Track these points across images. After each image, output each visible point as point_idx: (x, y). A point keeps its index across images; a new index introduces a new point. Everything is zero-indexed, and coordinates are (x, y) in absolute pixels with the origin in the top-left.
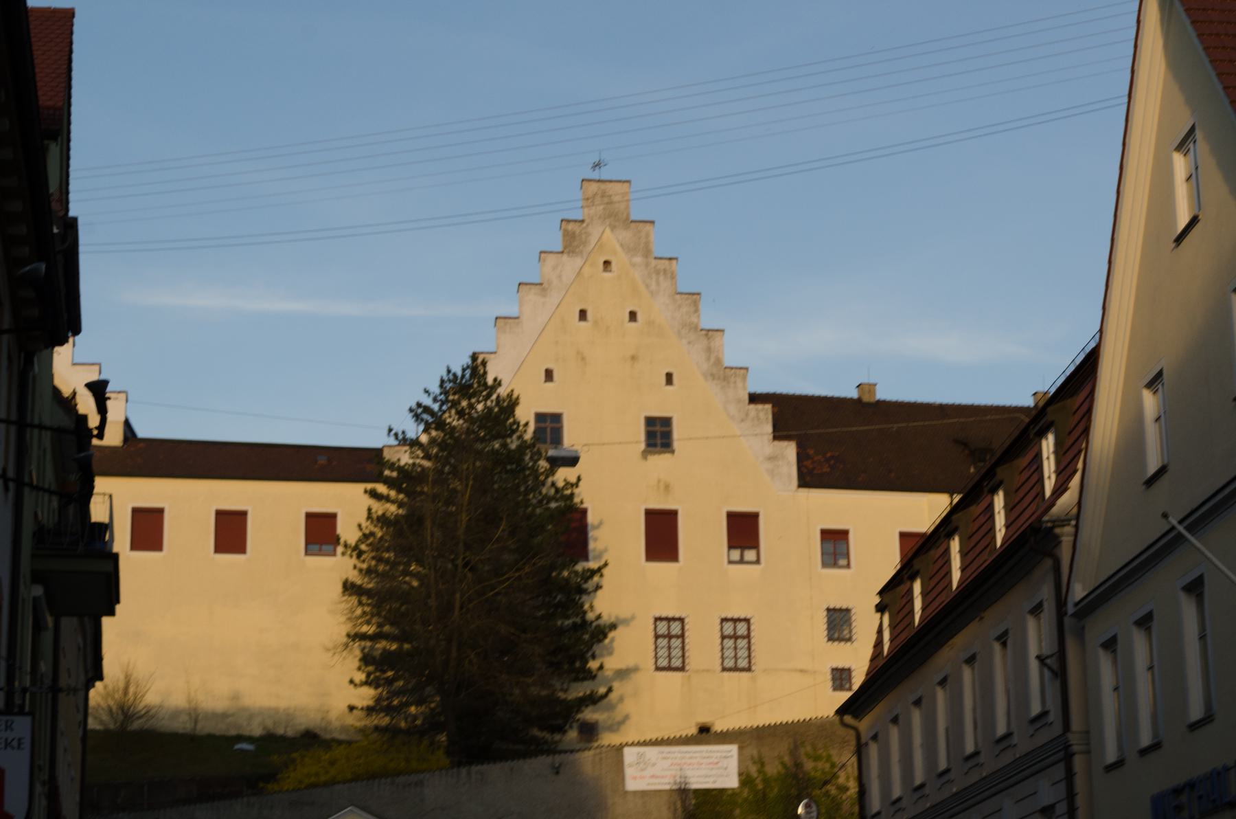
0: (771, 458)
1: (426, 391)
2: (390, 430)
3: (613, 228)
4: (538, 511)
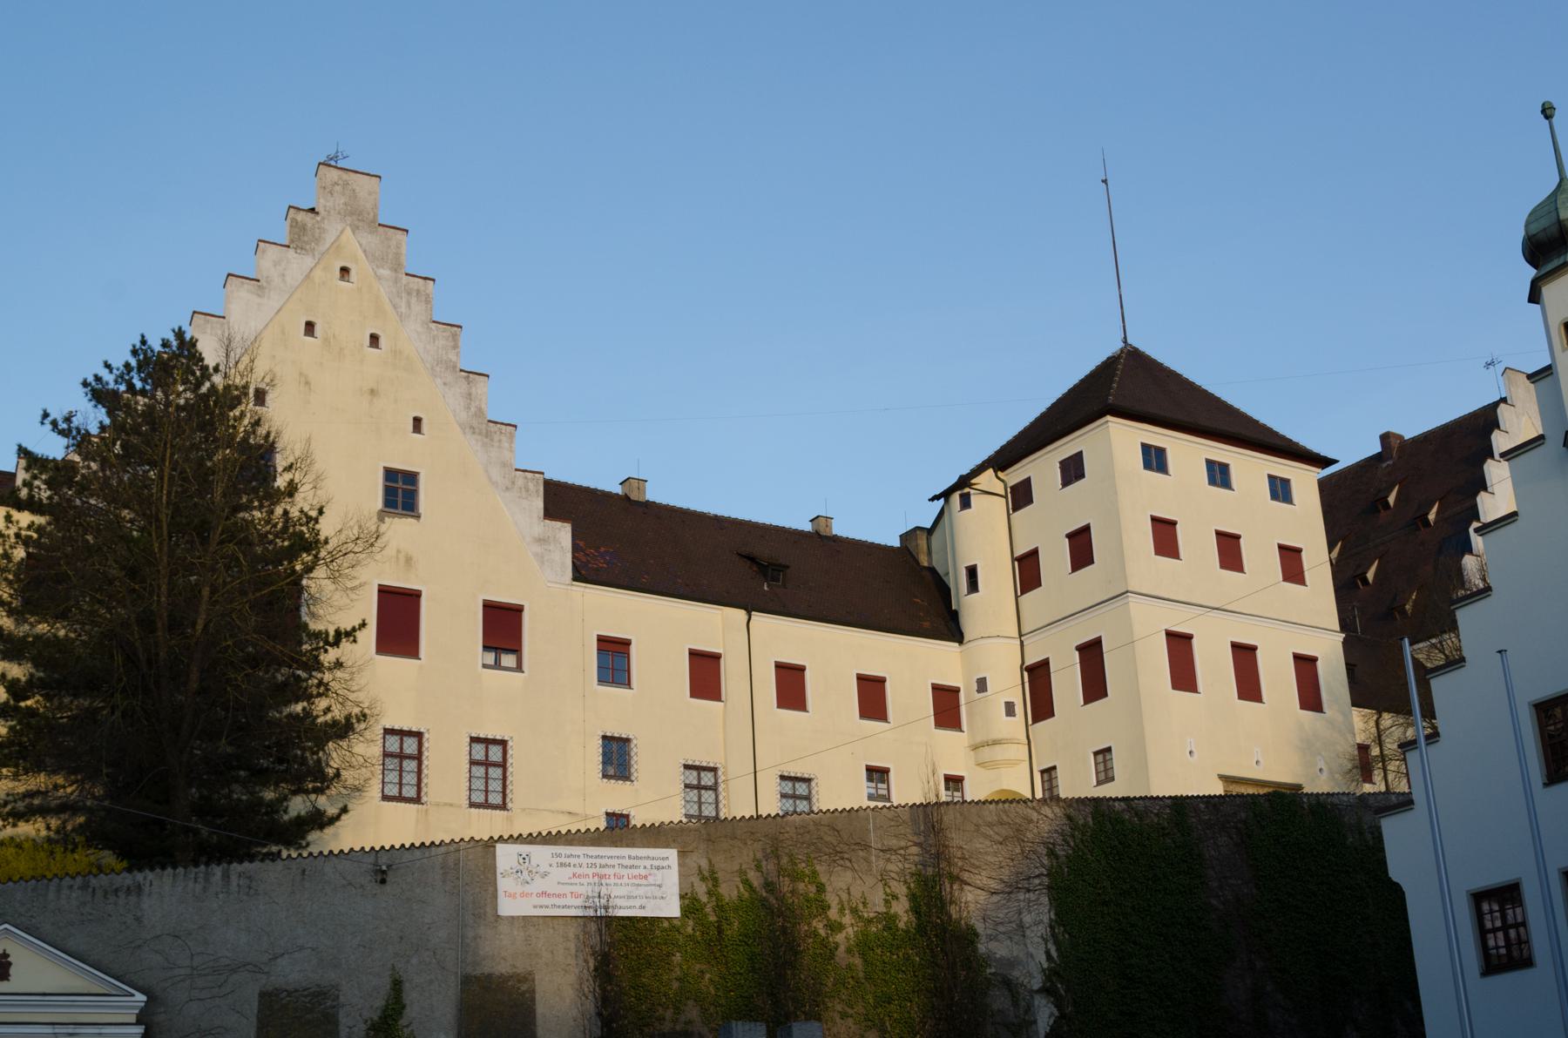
0: (541, 541)
1: (107, 366)
2: (46, 415)
3: (355, 229)
4: (66, 700)
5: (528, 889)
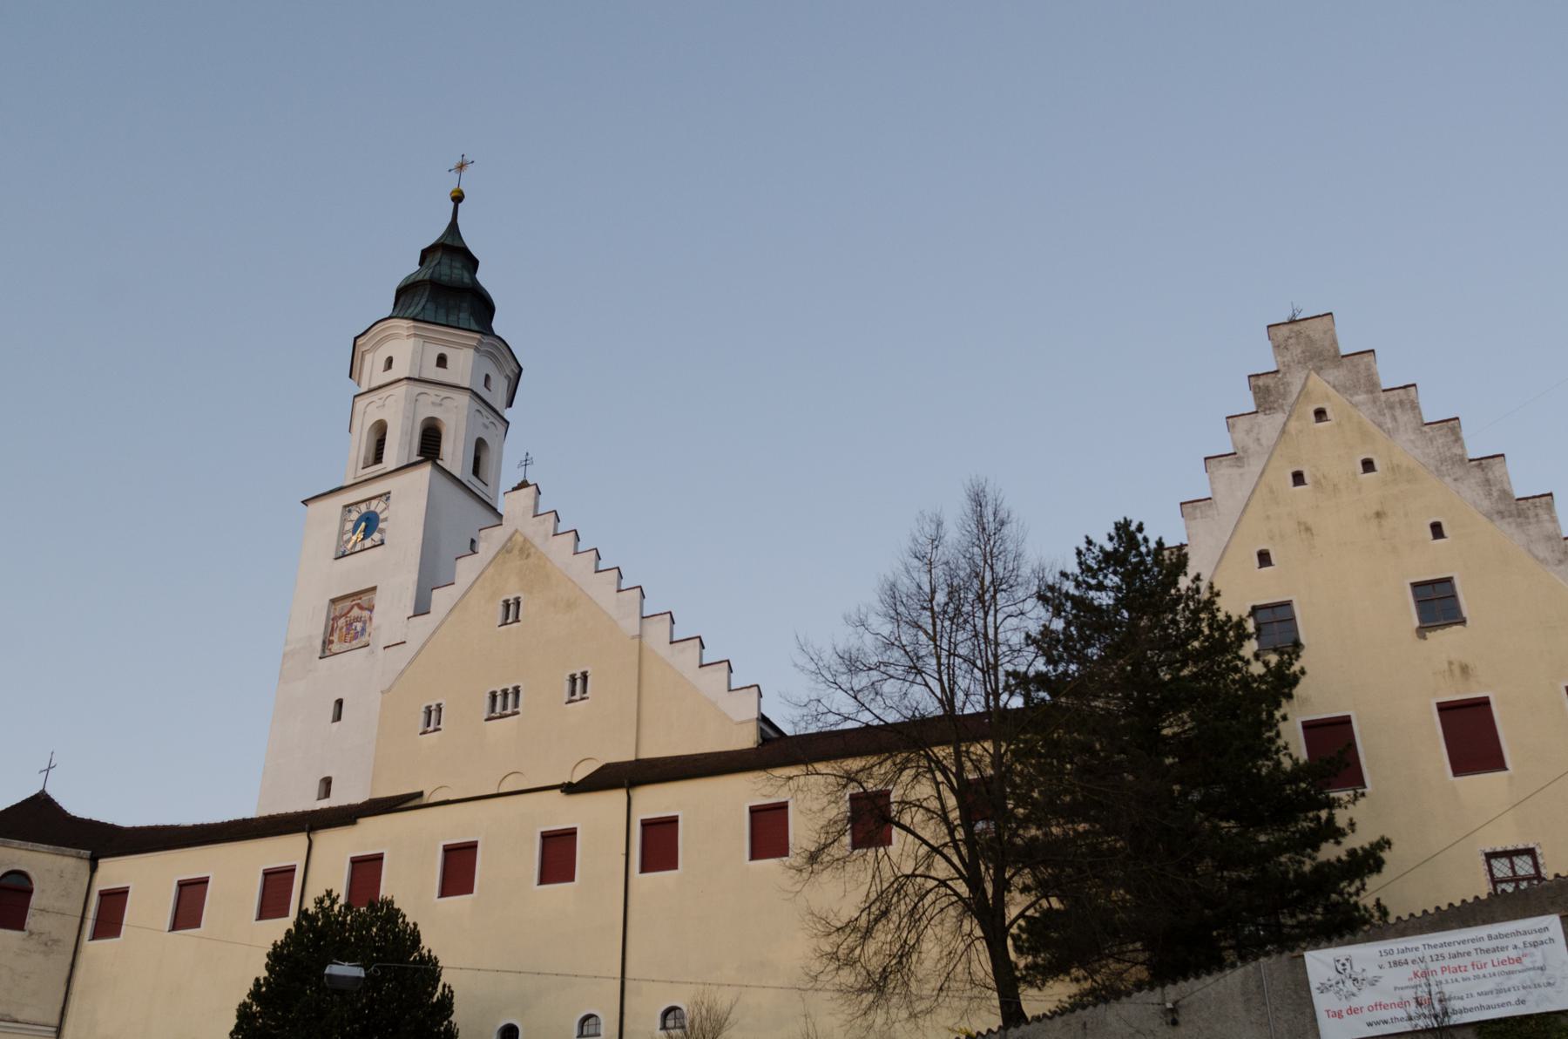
3: (1318, 370)
5: (1355, 1002)
